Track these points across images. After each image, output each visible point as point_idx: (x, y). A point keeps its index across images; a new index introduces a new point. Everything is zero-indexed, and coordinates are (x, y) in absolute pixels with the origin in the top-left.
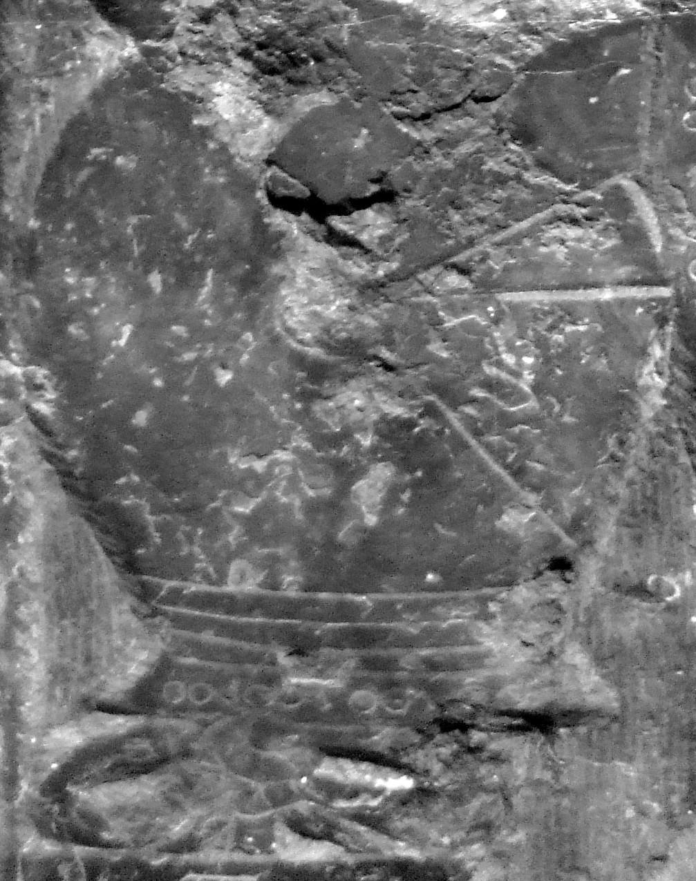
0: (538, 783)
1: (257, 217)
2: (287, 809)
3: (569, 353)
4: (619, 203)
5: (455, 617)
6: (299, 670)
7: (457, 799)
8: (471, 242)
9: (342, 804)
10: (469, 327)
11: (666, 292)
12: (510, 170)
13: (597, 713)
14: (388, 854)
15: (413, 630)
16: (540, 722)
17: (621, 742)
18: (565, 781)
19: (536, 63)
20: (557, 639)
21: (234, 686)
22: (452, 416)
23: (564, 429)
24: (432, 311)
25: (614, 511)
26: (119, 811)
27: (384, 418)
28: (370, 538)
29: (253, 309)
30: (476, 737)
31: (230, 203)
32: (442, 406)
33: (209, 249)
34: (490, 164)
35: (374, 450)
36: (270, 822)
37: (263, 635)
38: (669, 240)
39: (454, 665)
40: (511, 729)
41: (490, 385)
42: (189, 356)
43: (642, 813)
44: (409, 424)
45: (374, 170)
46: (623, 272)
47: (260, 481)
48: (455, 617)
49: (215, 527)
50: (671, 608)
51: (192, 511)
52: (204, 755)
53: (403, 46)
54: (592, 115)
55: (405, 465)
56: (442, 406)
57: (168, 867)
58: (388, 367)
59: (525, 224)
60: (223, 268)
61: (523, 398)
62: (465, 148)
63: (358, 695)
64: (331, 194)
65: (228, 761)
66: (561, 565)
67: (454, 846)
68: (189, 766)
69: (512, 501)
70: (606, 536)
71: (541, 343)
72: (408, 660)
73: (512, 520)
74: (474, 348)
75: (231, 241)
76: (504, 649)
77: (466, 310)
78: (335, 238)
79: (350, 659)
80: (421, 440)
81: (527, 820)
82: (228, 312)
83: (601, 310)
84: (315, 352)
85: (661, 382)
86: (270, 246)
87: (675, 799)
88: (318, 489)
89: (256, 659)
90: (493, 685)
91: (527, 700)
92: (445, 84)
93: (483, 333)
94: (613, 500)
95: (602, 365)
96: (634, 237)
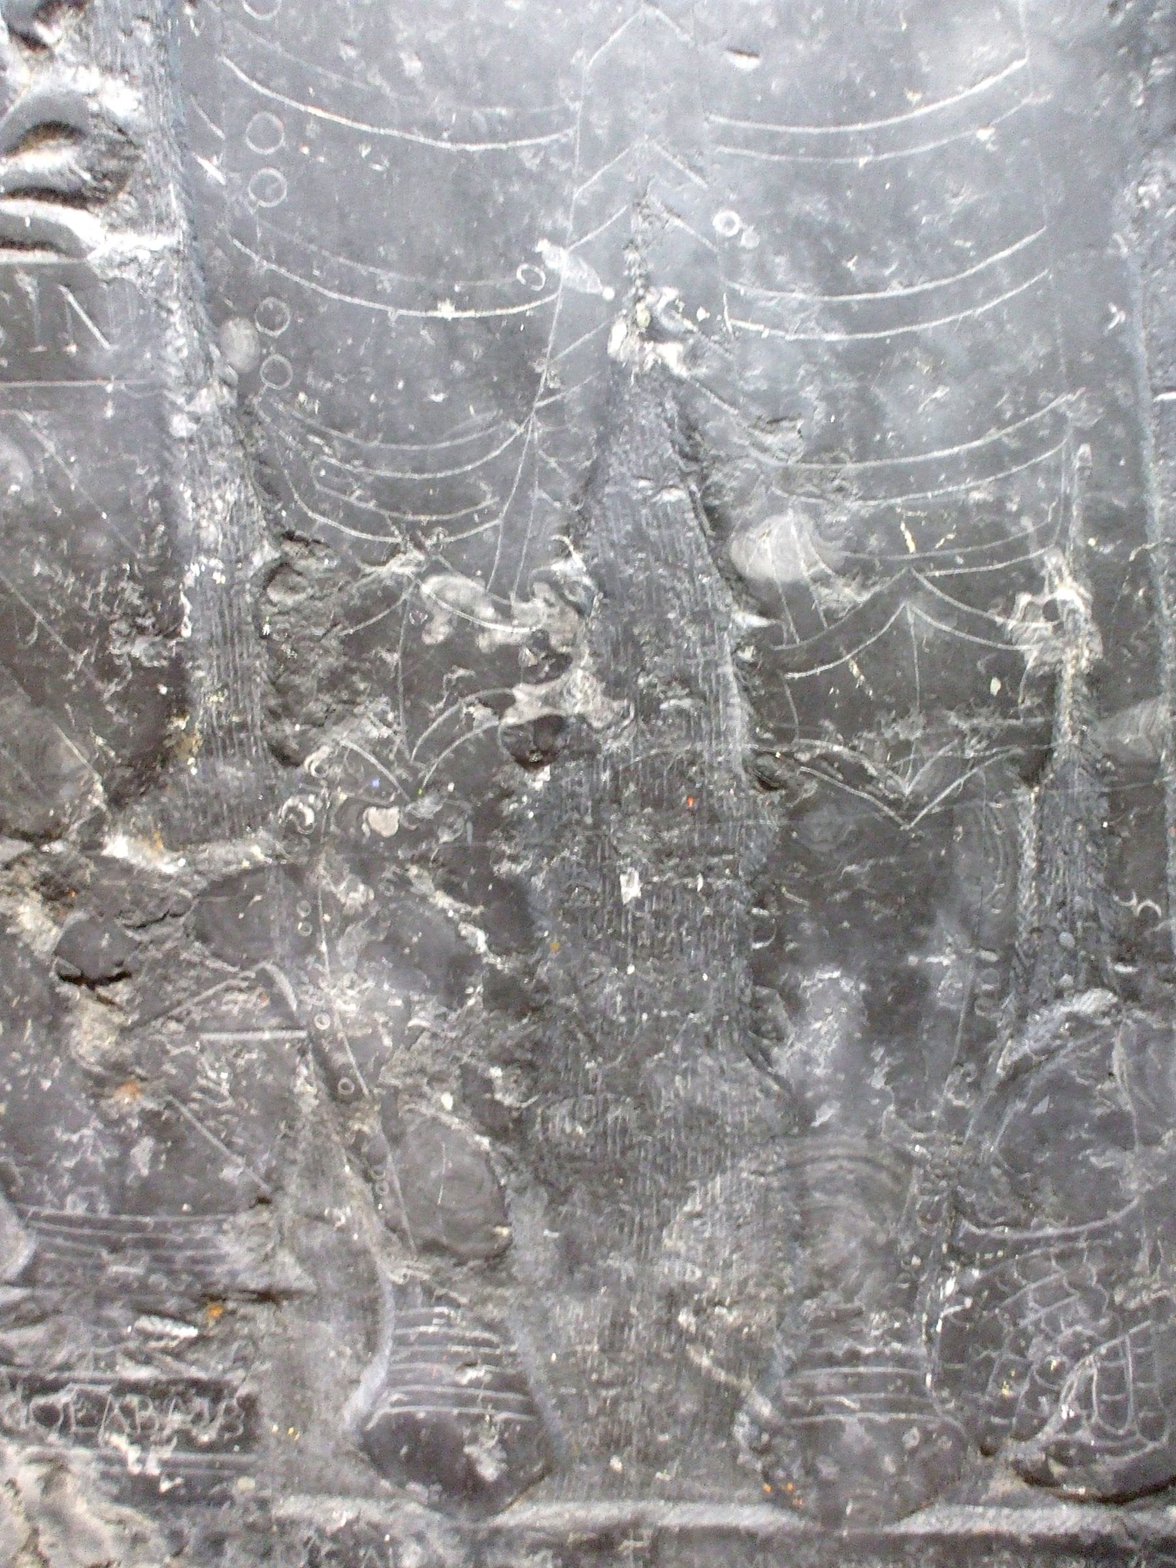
0: (273, 1335)
1: (52, 987)
2: (122, 1346)
3: (248, 1071)
4: (266, 980)
5: (204, 1232)
6: (115, 1263)
7: (224, 1342)
8: (179, 1003)
9: (153, 1344)
10: (185, 1055)
11: (303, 1034)
12: (196, 959)
13: (300, 1293)
14: (186, 1375)
15: (180, 1239)
16: (266, 1297)
17: (320, 1309)
18: (290, 1333)
19: (201, 894)
20: (270, 1246)
21: (79, 1271)
22: (184, 1109)
23: (253, 1119)
24: (162, 1045)
25: (295, 1170)
26: (23, 1346)
27: (143, 1110)
28: (145, 1185)
29: (57, 1042)
30: (231, 1305)
31: (35, 979)
32: (177, 1103)
33: (26, 1007)
34: (184, 955)
35: (140, 1129)
36: (113, 1354)
37: (90, 1240)
38: (300, 1002)
39: (208, 1261)
40: (253, 1301)
41: (203, 1090)
42: (24, 1072)
43: (340, 1354)
44: (158, 1114)
45: (117, 958)
46: (274, 1021)
47: (77, 1147)
48: (204, 1232)
49: (54, 1175)
50: (341, 1230)
51: (38, 1165)
52: (69, 1312)
53: (123, 883)
54: (241, 924)
55: (160, 1139)
56: (177, 1103)
57: (56, 1380)
58: (143, 1079)
59: (211, 992)
60: (36, 1018)
61: (223, 1099)
62: (169, 945)
63: (153, 1279)
64: (93, 974)
65: (84, 1315)
66: (263, 1201)
67: (225, 1371)
68: (62, 1319)
69: (227, 1161)
70: (293, 1185)
71: (231, 1065)
72: (180, 1257)
73: (229, 1173)
74: (190, 1068)
75: (38, 1001)
76: (236, 1252)
77: (183, 1043)
78: (101, 1000)
79: (145, 1257)
80: (167, 1122)
81: (270, 1356)
82: (42, 1045)
83: (264, 1046)
84: (98, 1069)
85: (311, 1090)
86: (62, 1006)
87: (359, 1346)
88: (109, 1152)
89: (90, 1255)
90: (233, 1274)
91: (256, 1283)
92: (151, 906)
93: (194, 1059)
94: (294, 1162)
95: (270, 1078)
96: (278, 1002)
